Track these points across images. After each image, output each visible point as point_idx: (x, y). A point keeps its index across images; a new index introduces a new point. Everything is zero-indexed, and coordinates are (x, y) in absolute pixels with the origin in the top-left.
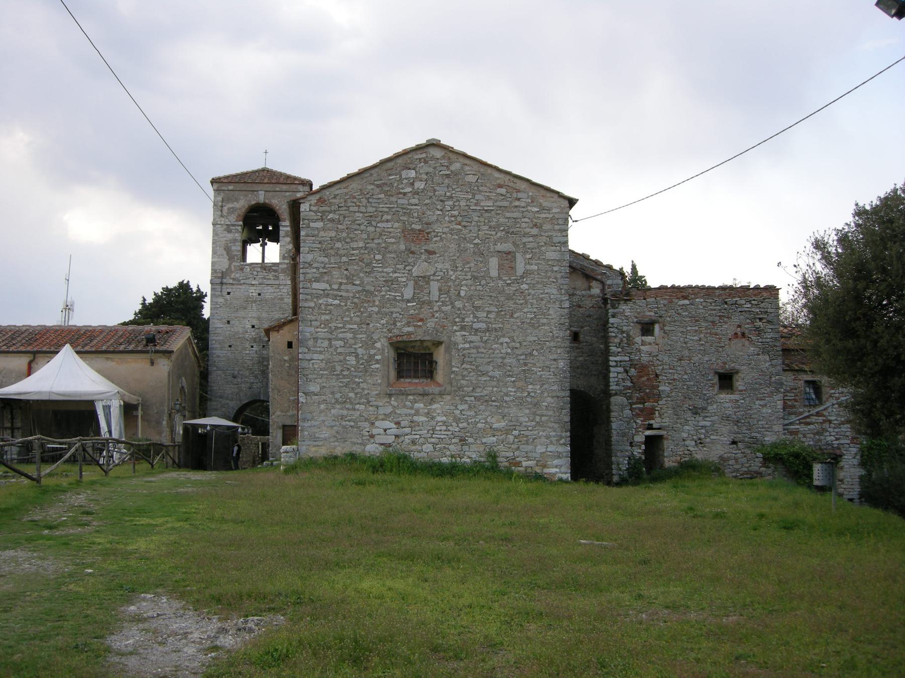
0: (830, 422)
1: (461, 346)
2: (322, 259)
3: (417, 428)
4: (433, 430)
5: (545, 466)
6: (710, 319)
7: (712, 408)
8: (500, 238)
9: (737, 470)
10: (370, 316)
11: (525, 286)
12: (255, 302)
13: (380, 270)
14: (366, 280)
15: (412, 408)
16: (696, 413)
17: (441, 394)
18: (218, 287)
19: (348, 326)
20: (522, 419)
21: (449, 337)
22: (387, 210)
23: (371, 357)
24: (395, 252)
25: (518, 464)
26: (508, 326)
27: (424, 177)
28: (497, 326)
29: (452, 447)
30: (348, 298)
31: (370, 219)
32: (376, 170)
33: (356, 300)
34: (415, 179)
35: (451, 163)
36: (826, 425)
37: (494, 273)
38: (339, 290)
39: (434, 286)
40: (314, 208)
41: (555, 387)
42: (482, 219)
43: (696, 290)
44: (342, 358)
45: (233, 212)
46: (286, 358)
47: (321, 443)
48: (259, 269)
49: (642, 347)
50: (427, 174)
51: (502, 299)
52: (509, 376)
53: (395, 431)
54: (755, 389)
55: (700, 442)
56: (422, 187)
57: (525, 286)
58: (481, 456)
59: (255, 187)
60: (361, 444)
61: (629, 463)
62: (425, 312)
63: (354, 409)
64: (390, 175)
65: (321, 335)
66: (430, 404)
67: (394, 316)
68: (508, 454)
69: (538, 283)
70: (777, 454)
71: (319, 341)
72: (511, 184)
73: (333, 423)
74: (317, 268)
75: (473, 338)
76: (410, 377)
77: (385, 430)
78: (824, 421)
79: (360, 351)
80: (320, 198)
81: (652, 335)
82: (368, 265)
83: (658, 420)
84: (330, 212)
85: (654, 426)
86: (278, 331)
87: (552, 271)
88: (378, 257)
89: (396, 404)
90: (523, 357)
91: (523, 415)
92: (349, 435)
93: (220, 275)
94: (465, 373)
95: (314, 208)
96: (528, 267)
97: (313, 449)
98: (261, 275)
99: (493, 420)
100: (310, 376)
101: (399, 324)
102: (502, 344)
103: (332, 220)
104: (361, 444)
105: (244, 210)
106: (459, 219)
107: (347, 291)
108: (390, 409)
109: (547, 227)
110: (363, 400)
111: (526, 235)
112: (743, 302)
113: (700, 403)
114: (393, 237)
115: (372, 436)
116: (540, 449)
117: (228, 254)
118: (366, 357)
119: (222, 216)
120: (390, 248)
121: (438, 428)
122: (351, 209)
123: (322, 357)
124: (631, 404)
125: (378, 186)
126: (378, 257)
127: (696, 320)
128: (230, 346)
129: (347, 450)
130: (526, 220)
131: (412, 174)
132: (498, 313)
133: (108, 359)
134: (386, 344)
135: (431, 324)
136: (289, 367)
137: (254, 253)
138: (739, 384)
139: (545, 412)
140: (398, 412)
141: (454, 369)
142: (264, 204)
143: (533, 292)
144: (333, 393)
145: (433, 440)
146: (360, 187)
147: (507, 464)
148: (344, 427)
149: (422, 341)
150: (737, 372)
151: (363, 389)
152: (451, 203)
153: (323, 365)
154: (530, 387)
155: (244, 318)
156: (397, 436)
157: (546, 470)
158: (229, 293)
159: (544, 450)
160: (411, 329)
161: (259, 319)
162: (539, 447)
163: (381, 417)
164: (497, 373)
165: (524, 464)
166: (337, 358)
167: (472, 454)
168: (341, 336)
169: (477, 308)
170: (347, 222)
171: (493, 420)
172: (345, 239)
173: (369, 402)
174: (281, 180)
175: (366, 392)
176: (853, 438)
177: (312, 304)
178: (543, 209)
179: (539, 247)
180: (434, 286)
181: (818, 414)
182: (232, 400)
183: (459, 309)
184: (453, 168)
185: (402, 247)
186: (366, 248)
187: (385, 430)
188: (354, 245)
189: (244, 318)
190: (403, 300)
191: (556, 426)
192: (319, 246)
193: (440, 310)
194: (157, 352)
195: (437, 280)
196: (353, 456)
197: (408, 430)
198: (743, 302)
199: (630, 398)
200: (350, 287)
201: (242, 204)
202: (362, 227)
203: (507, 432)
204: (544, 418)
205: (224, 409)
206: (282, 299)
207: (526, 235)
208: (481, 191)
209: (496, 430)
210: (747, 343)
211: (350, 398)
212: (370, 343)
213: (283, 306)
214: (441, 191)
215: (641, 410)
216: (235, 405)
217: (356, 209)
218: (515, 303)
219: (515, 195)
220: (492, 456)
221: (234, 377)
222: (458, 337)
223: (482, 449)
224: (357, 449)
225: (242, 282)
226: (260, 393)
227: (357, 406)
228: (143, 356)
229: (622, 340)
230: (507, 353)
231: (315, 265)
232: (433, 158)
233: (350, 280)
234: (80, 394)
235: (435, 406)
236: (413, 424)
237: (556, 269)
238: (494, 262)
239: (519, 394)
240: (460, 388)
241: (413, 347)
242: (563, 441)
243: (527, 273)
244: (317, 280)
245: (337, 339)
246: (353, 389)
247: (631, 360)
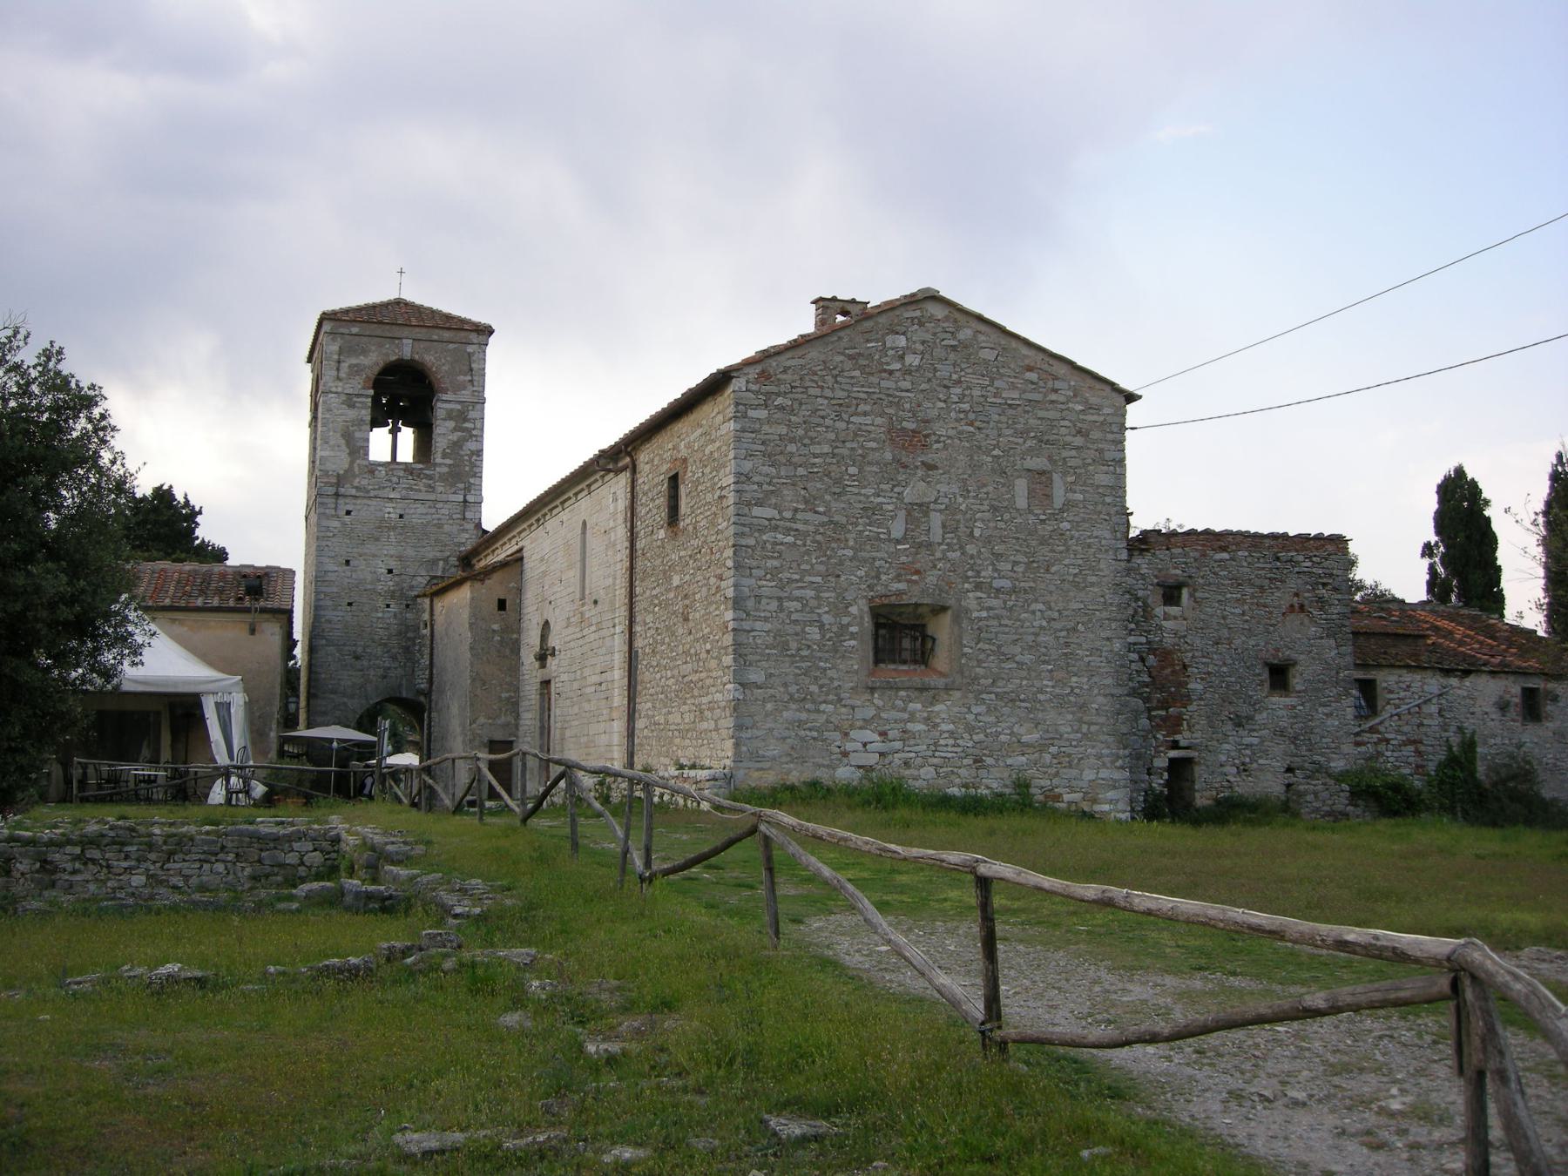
0: (1387, 741)
1: (975, 614)
2: (766, 469)
3: (912, 742)
4: (935, 744)
5: (1095, 801)
6: (1258, 582)
7: (1261, 717)
8: (1030, 449)
9: (1317, 810)
10: (841, 563)
11: (1065, 525)
12: (394, 528)
13: (856, 490)
14: (835, 506)
15: (904, 710)
16: (1239, 725)
17: (947, 689)
18: (331, 501)
19: (808, 578)
20: (1062, 729)
21: (959, 600)
22: (863, 396)
23: (844, 628)
24: (878, 463)
25: (1058, 798)
26: (1043, 586)
27: (920, 347)
28: (1026, 585)
29: (962, 772)
30: (807, 534)
31: (840, 408)
32: (848, 331)
33: (819, 537)
34: (906, 350)
35: (958, 328)
36: (1382, 747)
37: (1022, 503)
38: (793, 520)
39: (936, 519)
40: (754, 387)
41: (1109, 681)
42: (1003, 419)
43: (1239, 538)
44: (798, 628)
45: (358, 373)
46: (496, 627)
47: (768, 765)
48: (401, 474)
49: (1165, 623)
50: (923, 343)
51: (1034, 543)
52: (1044, 662)
53: (879, 746)
54: (1318, 690)
55: (1243, 769)
56: (916, 363)
57: (1065, 525)
58: (1006, 786)
59: (397, 332)
60: (828, 766)
61: (1145, 801)
62: (923, 559)
63: (818, 711)
64: (868, 341)
65: (765, 591)
66: (932, 704)
67: (877, 563)
68: (1043, 783)
69: (1084, 520)
70: (1369, 786)
71: (764, 601)
72: (1045, 367)
73: (787, 733)
74: (760, 484)
75: (995, 603)
76: (894, 662)
77: (865, 745)
78: (1380, 740)
79: (827, 619)
80: (763, 372)
81: (1178, 605)
82: (838, 482)
83: (1187, 734)
84: (778, 394)
85: (1182, 743)
86: (482, 581)
87: (1104, 503)
88: (852, 470)
89: (881, 703)
90: (1064, 633)
91: (1065, 723)
92: (811, 752)
93: (334, 480)
94: (982, 656)
95: (754, 387)
96: (1070, 495)
97: (756, 774)
98: (405, 483)
99: (1022, 730)
100: (750, 657)
101: (884, 577)
102: (1033, 612)
103: (781, 408)
104: (828, 766)
105: (377, 370)
106: (972, 416)
107: (806, 522)
108: (871, 712)
109: (1095, 435)
110: (831, 697)
111: (1066, 446)
112: (1301, 558)
113: (1244, 710)
114: (874, 440)
115: (845, 754)
116: (1089, 775)
117: (348, 444)
118: (835, 629)
119: (339, 379)
120: (870, 458)
121: (942, 742)
122: (812, 391)
123: (768, 626)
124: (1149, 710)
125: (851, 357)
126: (852, 470)
127: (1238, 582)
128: (350, 604)
129: (808, 775)
130: (1066, 423)
131: (902, 341)
132: (1028, 564)
133: (173, 621)
134: (866, 609)
135: (931, 579)
136: (501, 642)
137: (379, 444)
138: (1296, 682)
139: (1095, 719)
140: (884, 715)
141: (967, 650)
142: (412, 360)
143: (1077, 534)
144: (785, 685)
145: (935, 761)
146: (822, 357)
147: (1041, 798)
148: (802, 739)
149: (917, 605)
150: (1295, 663)
151: (832, 679)
152: (959, 391)
153: (770, 640)
154: (1074, 679)
155: (374, 556)
156: (882, 754)
157: (1097, 808)
158: (348, 513)
159: (1092, 777)
160: (902, 586)
161: (400, 558)
162: (1086, 772)
163: (859, 724)
164: (1027, 658)
165: (1066, 797)
166: (791, 629)
167: (993, 782)
168: (797, 593)
169: (998, 556)
170: (804, 412)
171: (1022, 730)
172: (801, 438)
173: (840, 700)
174: (441, 324)
175: (836, 684)
176: (1418, 767)
177: (752, 542)
178: (1090, 408)
179: (1085, 465)
180: (936, 519)
181: (1372, 730)
182: (352, 697)
183: (972, 557)
184: (961, 336)
185: (888, 456)
186: (834, 455)
187: (865, 745)
188: (816, 449)
189: (374, 556)
190: (890, 540)
191: (1111, 739)
192: (762, 448)
193: (944, 558)
194: (264, 610)
195: (940, 511)
196: (814, 784)
197: (898, 745)
198: (1301, 558)
199: (1147, 700)
200: (810, 516)
201: (374, 359)
202: (828, 422)
203: (1042, 748)
204: (1093, 728)
205: (338, 713)
206: (440, 526)
207: (1066, 446)
208: (1002, 375)
209: (1027, 745)
210: (1306, 621)
211: (811, 694)
212: (840, 607)
213: (443, 537)
214: (944, 371)
215: (1164, 719)
216: (357, 706)
217: (817, 392)
218: (1053, 551)
219: (1050, 384)
220: (1022, 786)
221: (357, 658)
222: (971, 601)
223: (1006, 775)
224: (823, 775)
225: (372, 494)
226: (400, 685)
227: (823, 707)
228: (237, 616)
229: (1136, 611)
230: (1041, 628)
231: (755, 479)
232: (932, 318)
233: (810, 504)
234: (176, 682)
235: (938, 707)
236: (906, 735)
237: (1108, 500)
238: (1021, 486)
239: (1057, 690)
240: (976, 678)
241: (900, 614)
242: (1119, 763)
243: (1068, 505)
244: (759, 503)
245: (790, 599)
246: (816, 678)
247: (1149, 643)
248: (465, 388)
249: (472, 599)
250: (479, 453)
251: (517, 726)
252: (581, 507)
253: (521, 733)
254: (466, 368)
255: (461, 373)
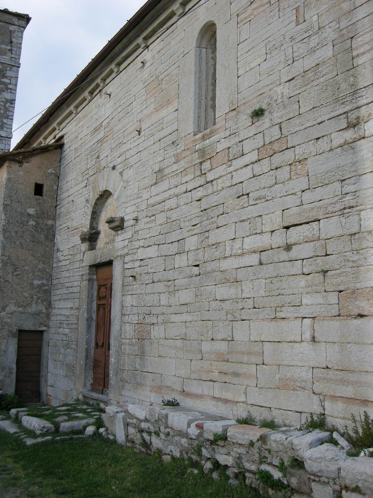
46: (31, 211)
86: (20, 163)
248: (5, 54)
249: (9, 180)
250: (12, 102)
251: (48, 316)
252: (127, 82)
253: (54, 320)
254: (7, 40)
255: (3, 43)
